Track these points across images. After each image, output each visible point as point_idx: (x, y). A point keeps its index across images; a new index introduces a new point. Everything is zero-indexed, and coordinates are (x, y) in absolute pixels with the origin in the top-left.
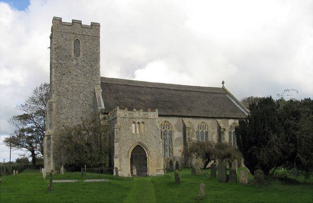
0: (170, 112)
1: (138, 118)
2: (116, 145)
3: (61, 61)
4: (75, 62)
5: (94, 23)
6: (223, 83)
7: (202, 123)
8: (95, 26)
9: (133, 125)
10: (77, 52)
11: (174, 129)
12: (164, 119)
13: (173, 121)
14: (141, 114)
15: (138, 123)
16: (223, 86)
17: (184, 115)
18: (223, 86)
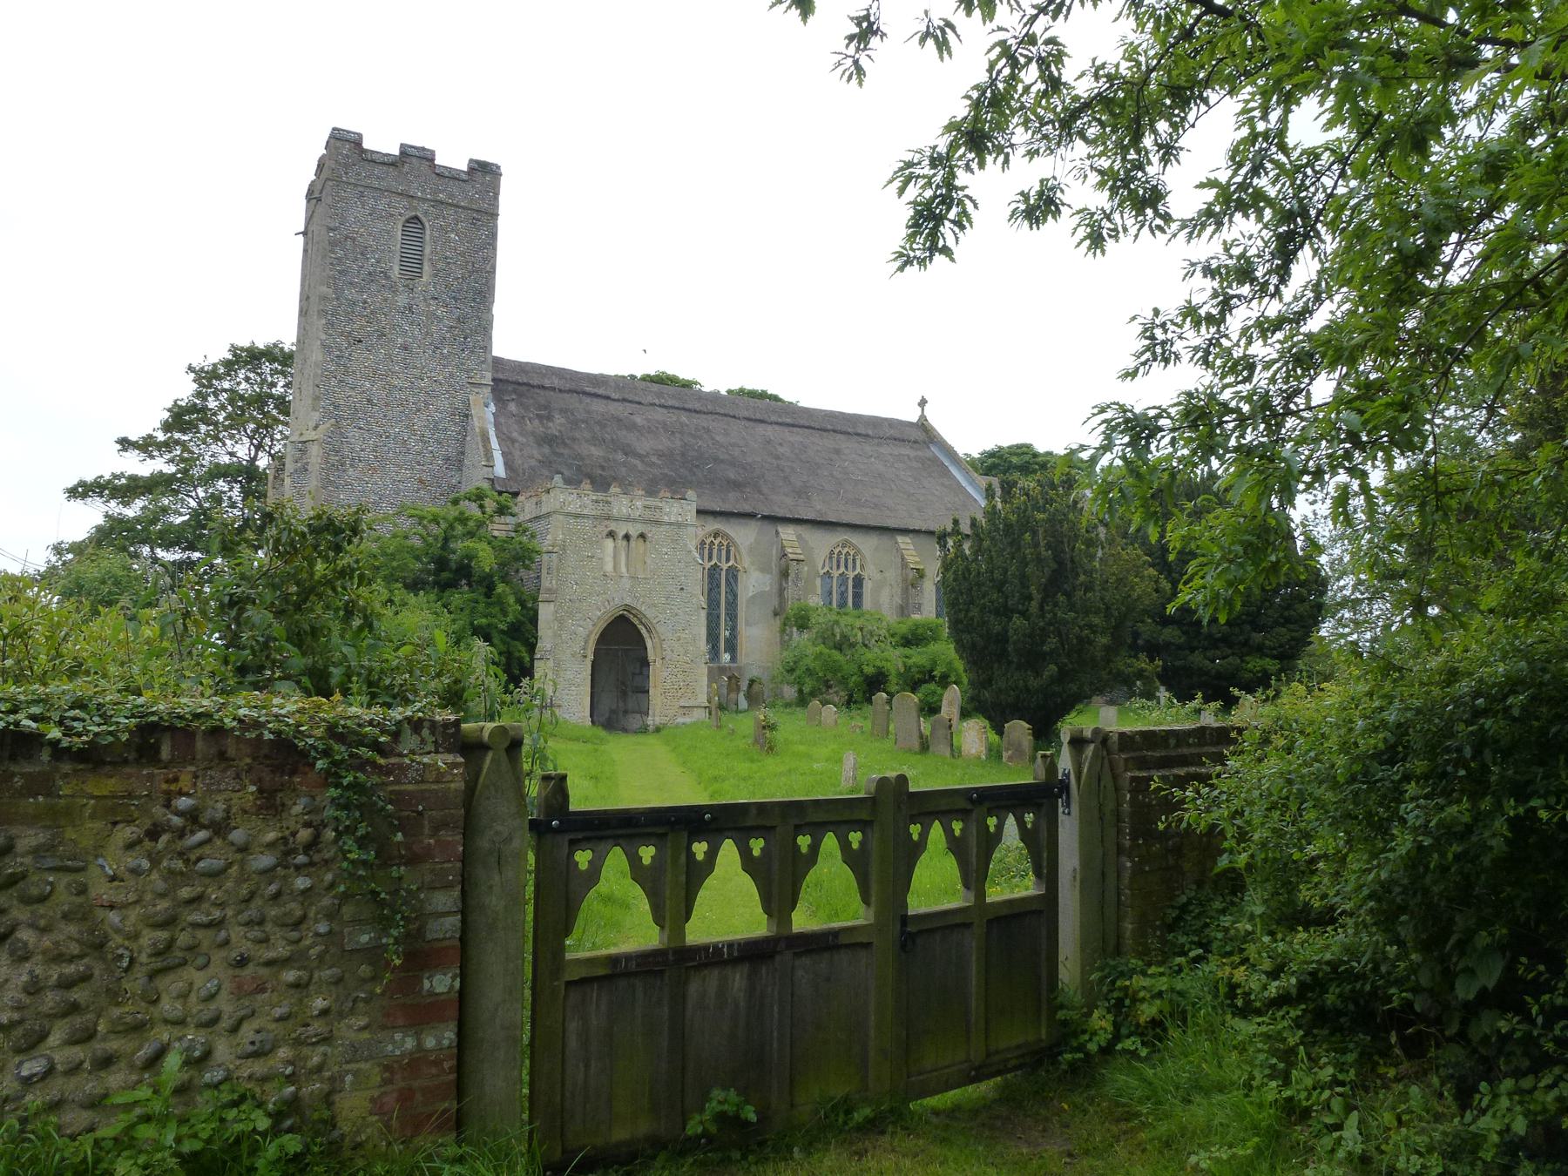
0: (732, 503)
1: (628, 519)
2: (545, 612)
3: (350, 293)
4: (402, 300)
5: (477, 162)
6: (923, 403)
7: (716, 535)
8: (484, 174)
9: (609, 543)
10: (413, 267)
11: (746, 562)
12: (714, 525)
13: (744, 535)
14: (639, 504)
15: (627, 537)
16: (923, 417)
17: (781, 513)
18: (923, 417)
